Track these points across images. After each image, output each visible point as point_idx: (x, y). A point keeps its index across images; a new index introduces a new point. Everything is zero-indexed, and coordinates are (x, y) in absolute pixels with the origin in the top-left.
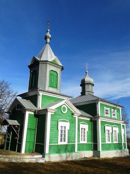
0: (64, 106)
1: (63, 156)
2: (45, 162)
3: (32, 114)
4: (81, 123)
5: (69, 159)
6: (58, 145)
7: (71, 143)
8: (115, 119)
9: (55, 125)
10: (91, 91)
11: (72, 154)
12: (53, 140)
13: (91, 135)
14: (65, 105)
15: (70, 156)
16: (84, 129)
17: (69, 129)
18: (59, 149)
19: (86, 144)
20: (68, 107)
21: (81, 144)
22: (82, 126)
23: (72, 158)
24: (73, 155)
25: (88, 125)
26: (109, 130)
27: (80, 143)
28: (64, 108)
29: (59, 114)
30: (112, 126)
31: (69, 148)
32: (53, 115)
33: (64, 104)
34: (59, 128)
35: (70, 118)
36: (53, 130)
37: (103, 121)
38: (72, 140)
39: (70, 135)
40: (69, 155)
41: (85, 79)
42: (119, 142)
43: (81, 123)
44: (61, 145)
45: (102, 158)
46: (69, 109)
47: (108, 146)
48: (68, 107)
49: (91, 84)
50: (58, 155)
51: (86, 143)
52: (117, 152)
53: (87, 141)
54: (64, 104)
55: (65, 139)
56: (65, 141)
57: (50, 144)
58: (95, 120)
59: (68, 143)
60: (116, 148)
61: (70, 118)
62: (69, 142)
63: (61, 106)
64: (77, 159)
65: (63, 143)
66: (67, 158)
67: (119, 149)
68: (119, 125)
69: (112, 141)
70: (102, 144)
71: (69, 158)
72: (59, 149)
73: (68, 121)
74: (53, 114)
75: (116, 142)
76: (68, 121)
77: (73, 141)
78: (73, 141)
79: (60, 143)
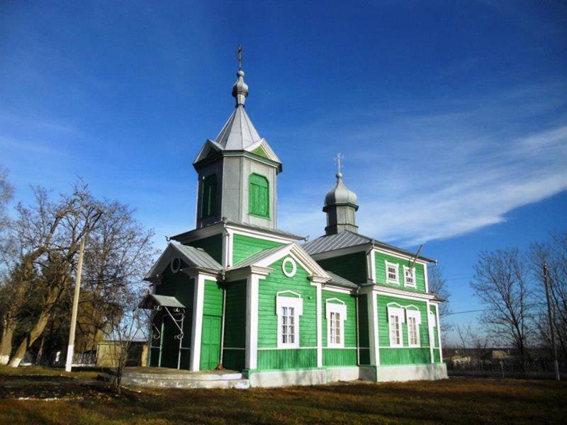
2: (250, 387)
4: (328, 302)
16: (338, 315)
18: (281, 360)
20: (297, 263)
23: (311, 380)
26: (397, 317)
28: (289, 266)
29: (276, 279)
30: (406, 307)
31: (303, 358)
33: (289, 256)
34: (280, 312)
36: (265, 316)
40: (304, 374)
42: (421, 344)
43: (328, 302)
44: (284, 351)
46: (299, 267)
47: (394, 353)
48: (297, 263)
51: (402, 347)
53: (345, 343)
54: (289, 256)
58: (363, 293)
59: (300, 346)
62: (302, 344)
63: (281, 261)
64: (321, 383)
69: (406, 343)
72: (281, 360)
73: (300, 295)
74: (264, 278)
76: (300, 295)
77: (311, 341)
79: (281, 346)
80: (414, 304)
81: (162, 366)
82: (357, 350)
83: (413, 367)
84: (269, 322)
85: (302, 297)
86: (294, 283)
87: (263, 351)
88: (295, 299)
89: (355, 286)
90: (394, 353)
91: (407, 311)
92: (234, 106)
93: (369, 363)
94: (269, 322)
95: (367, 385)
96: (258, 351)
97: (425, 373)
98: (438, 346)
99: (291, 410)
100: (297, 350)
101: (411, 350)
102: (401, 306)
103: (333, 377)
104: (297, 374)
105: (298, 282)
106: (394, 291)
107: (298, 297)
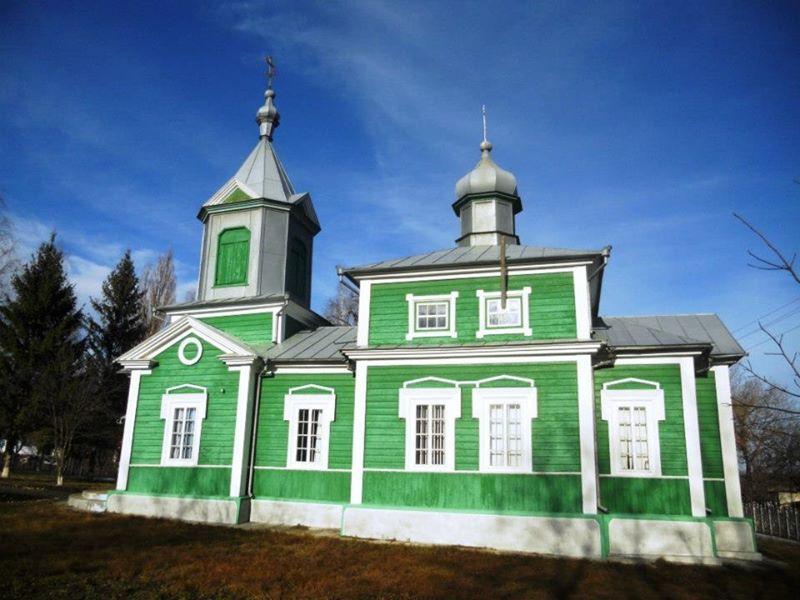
0: (192, 340)
1: (166, 503)
2: (106, 511)
3: (344, 374)
5: (192, 517)
6: (402, 473)
7: (212, 464)
8: (441, 345)
9: (152, 408)
11: (207, 503)
12: (143, 451)
13: (260, 427)
14: (182, 340)
15: (197, 508)
18: (164, 482)
19: (324, 473)
22: (612, 400)
23: (205, 515)
24: (210, 507)
25: (662, 392)
26: (492, 407)
29: (169, 371)
31: (205, 481)
35: (217, 377)
36: (147, 422)
37: (395, 367)
38: (220, 453)
40: (193, 504)
41: (469, 183)
42: (539, 462)
44: (173, 469)
45: (345, 537)
49: (476, 198)
50: (544, 519)
53: (457, 463)
57: (130, 462)
59: (199, 463)
61: (217, 377)
62: (202, 458)
64: (225, 521)
65: (179, 462)
66: (183, 510)
67: (546, 509)
68: (386, 382)
70: (366, 474)
71: (192, 512)
72: (164, 482)
77: (222, 456)
78: (222, 456)
79: (166, 462)
81: (366, 499)
82: (254, 465)
84: (152, 430)
85: (661, 388)
86: (199, 372)
87: (138, 468)
88: (652, 391)
90: (417, 484)
93: (582, 512)
94: (152, 430)
95: (623, 565)
96: (130, 468)
98: (348, 462)
100: (195, 470)
102: (457, 383)
105: (207, 369)
107: (654, 387)
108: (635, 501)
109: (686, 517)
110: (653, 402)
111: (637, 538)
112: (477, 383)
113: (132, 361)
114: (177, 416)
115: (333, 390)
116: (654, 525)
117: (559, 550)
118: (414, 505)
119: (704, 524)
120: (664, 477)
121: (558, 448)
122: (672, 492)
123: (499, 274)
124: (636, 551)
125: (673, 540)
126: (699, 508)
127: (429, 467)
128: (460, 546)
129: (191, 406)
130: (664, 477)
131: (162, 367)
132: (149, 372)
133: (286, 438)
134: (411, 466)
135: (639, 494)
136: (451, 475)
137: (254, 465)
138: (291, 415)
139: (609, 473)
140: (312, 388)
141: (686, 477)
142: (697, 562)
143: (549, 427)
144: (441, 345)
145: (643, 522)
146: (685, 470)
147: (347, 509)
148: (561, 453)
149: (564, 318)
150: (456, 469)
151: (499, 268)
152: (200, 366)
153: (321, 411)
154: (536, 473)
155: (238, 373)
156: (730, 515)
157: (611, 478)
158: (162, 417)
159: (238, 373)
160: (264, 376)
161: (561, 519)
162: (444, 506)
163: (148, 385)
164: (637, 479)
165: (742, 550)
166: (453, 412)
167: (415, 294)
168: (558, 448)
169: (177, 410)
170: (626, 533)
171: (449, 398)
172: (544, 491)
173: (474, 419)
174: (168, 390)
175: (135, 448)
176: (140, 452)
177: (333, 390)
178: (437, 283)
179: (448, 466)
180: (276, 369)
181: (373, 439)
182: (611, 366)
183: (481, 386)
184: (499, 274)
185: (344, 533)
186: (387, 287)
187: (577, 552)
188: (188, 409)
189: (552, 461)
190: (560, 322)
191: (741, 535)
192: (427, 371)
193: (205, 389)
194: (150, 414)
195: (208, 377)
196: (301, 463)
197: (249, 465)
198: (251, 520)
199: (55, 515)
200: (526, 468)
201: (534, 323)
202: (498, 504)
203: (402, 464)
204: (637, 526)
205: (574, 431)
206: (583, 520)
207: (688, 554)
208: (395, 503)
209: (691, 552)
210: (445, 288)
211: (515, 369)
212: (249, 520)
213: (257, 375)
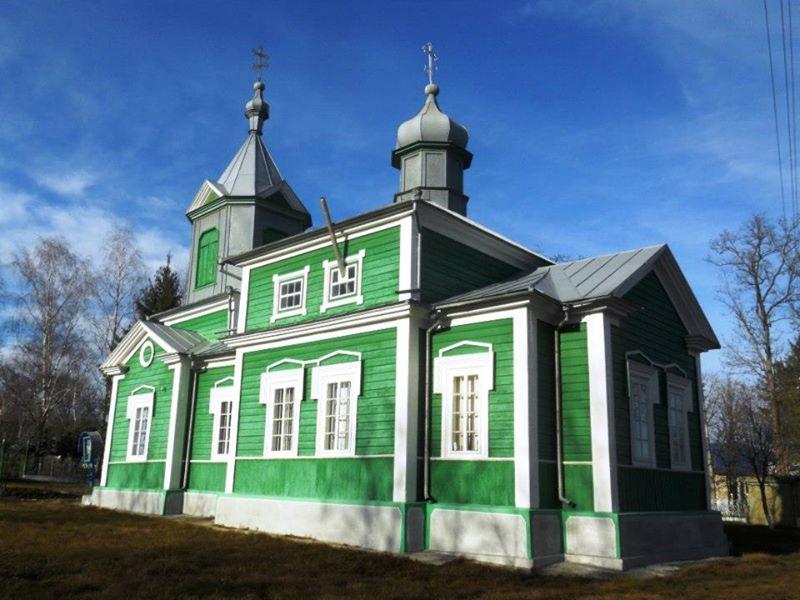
8: (352, 311)
10: (349, 249)
17: (692, 410)
21: (266, 460)
23: (145, 506)
24: (148, 498)
27: (264, 457)
30: (666, 367)
31: (151, 474)
32: (123, 380)
35: (161, 376)
37: (261, 352)
39: (156, 434)
42: (361, 446)
44: (133, 464)
47: (272, 472)
51: (296, 457)
52: (326, 512)
55: (471, 438)
56: (289, 448)
59: (148, 458)
60: (333, 491)
61: (161, 376)
66: (134, 502)
69: (307, 444)
75: (337, 453)
80: (292, 356)
81: (234, 489)
82: (430, 455)
83: (314, 505)
88: (681, 378)
89: (556, 333)
90: (272, 472)
91: (670, 376)
92: (441, 92)
93: (391, 499)
97: (351, 524)
99: (345, 583)
101: (322, 463)
103: (205, 509)
104: (133, 495)
106: (270, 336)
108: (462, 488)
109: (590, 513)
110: (480, 364)
111: (456, 531)
112: (318, 361)
113: (111, 367)
114: (457, 388)
115: (490, 346)
116: (471, 516)
117: (367, 543)
118: (268, 493)
119: (520, 516)
120: (491, 459)
121: (378, 427)
122: (497, 478)
123: (330, 243)
124: (366, 539)
125: (490, 536)
126: (523, 498)
127: (282, 454)
128: (291, 536)
129: (471, 374)
130: (491, 459)
131: (132, 371)
132: (123, 377)
133: (211, 431)
134: (269, 454)
135: (468, 479)
136: (294, 460)
137: (563, 459)
138: (215, 408)
139: (439, 455)
140: (464, 346)
141: (542, 461)
142: (509, 564)
143: (371, 405)
144: (352, 311)
145: (464, 513)
146: (510, 450)
147: (220, 498)
148: (380, 434)
149: (390, 279)
150: (490, 456)
151: (329, 237)
152: (153, 367)
153: (477, 376)
154: (357, 456)
155: (394, 330)
156: (596, 510)
157: (441, 461)
158: (261, 402)
159: (394, 330)
160: (435, 332)
161: (372, 507)
162: (289, 495)
163: (124, 388)
164: (468, 462)
165: (604, 555)
166: (485, 383)
167: (279, 274)
168: (378, 427)
169: (458, 380)
170: (446, 524)
171: (292, 378)
172: (365, 476)
173: (437, 395)
174: (216, 383)
175: (240, 446)
176: (116, 451)
177: (490, 346)
178: (300, 258)
179: (292, 454)
180: (207, 364)
181: (245, 427)
182: (447, 329)
183: (321, 364)
184: (330, 243)
185: (217, 521)
186: (282, 264)
187: (381, 546)
188: (288, 390)
189: (374, 442)
190: (386, 284)
191: (605, 537)
192: (280, 353)
193: (359, 354)
194: (121, 411)
195: (156, 377)
196: (134, 456)
197: (184, 457)
198: (184, 511)
199: (537, 576)
200: (350, 452)
201: (367, 289)
202: (328, 490)
203: (261, 450)
204: (457, 515)
205: (390, 407)
206: (390, 508)
207: (501, 554)
208: (256, 493)
209: (506, 551)
210: (298, 265)
211: (353, 341)
212: (181, 513)
213: (422, 333)
